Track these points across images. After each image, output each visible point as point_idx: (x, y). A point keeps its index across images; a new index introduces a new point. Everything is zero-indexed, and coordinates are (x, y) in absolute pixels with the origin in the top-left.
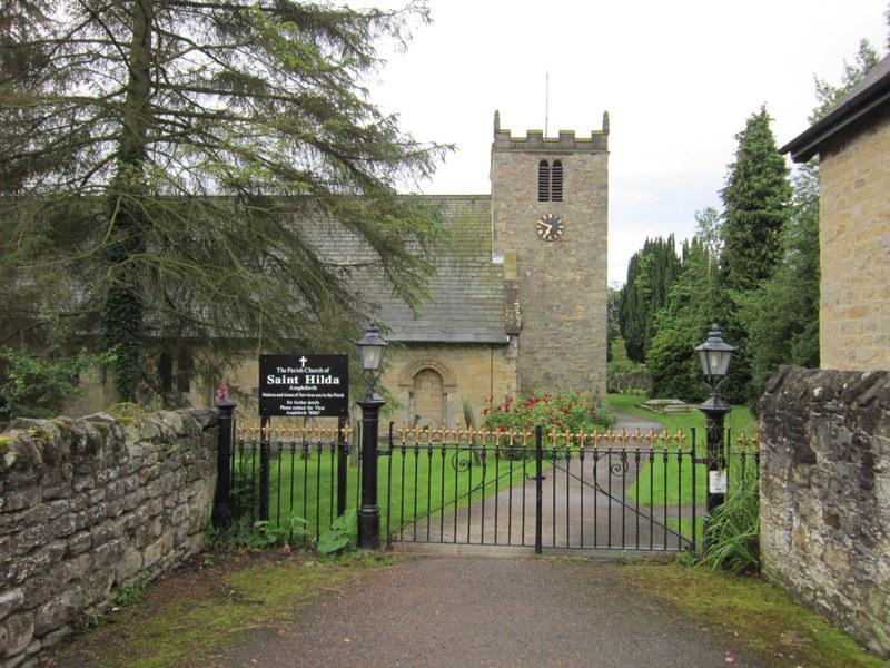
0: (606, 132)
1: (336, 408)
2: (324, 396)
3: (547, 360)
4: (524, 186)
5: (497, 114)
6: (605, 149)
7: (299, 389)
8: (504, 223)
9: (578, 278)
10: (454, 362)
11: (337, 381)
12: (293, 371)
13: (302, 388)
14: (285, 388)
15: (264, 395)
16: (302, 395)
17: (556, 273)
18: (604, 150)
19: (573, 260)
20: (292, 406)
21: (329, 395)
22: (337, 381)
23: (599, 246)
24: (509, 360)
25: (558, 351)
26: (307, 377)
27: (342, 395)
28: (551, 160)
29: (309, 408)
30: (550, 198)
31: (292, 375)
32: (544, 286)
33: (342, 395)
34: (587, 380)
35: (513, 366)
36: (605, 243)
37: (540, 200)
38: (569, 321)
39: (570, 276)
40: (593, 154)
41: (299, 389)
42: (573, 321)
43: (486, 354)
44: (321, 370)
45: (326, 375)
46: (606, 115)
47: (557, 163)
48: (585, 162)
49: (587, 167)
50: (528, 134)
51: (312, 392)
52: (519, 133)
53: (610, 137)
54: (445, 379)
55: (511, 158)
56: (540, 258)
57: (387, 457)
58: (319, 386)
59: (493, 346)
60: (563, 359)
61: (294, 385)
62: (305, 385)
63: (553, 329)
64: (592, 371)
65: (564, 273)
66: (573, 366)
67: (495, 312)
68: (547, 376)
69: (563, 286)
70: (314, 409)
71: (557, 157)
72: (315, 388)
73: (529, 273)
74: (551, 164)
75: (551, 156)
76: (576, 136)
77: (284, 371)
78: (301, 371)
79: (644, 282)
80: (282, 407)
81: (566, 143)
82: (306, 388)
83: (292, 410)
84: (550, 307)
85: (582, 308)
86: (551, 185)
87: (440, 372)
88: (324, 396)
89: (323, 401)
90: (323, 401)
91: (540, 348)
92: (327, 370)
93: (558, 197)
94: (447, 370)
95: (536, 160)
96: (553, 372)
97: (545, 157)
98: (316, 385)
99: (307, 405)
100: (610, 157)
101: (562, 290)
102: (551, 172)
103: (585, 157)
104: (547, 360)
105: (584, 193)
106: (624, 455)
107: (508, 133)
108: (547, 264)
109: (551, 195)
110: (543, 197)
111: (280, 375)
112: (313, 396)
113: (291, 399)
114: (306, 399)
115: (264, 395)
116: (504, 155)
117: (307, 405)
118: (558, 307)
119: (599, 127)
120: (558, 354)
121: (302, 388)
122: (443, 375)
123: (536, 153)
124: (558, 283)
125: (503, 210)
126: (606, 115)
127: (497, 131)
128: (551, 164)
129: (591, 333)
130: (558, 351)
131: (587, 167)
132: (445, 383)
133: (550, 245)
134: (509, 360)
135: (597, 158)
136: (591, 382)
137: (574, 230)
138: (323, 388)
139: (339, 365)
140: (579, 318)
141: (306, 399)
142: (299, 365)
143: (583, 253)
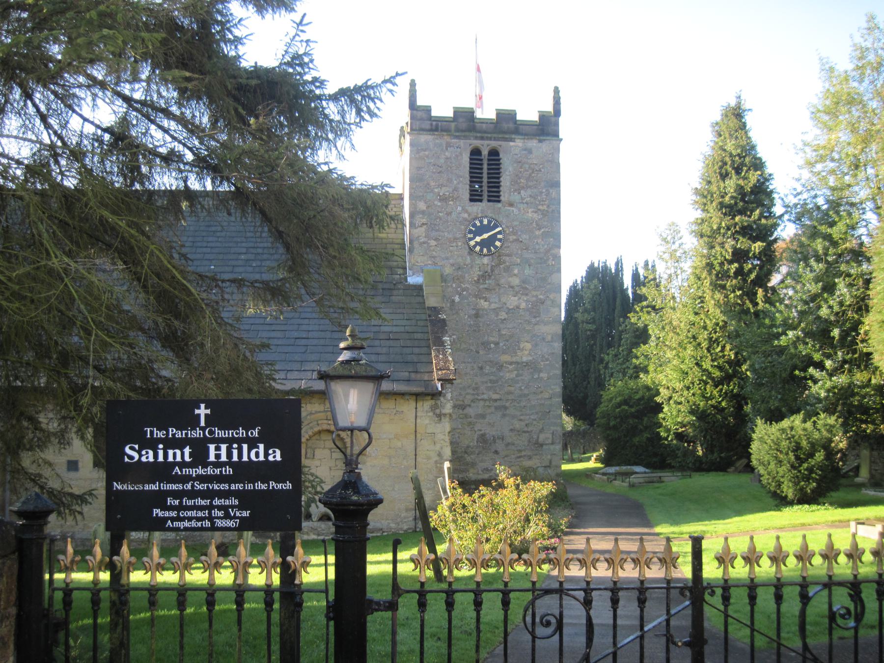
0: (557, 112)
2: (250, 487)
3: (483, 416)
4: (450, 180)
6: (556, 134)
8: (423, 229)
9: (523, 305)
12: (179, 435)
13: (200, 471)
14: (162, 471)
16: (199, 487)
18: (554, 134)
20: (178, 508)
22: (276, 455)
23: (550, 262)
24: (440, 416)
25: (498, 404)
26: (212, 447)
27: (289, 486)
29: (217, 513)
30: (485, 197)
31: (179, 444)
32: (477, 316)
33: (289, 486)
34: (537, 443)
35: (446, 426)
36: (557, 258)
37: (471, 200)
38: (511, 363)
39: (512, 301)
40: (540, 141)
42: (518, 363)
44: (242, 433)
46: (556, 91)
47: (494, 153)
48: (530, 151)
50: (455, 112)
51: (220, 479)
52: (443, 110)
53: (561, 120)
57: (389, 614)
60: (504, 415)
61: (183, 464)
62: (205, 465)
64: (542, 431)
66: (517, 425)
67: (416, 350)
68: (483, 438)
70: (227, 516)
71: (494, 144)
72: (229, 471)
73: (457, 299)
74: (485, 152)
75: (486, 142)
76: (519, 118)
77: (161, 434)
78: (197, 434)
79: (586, 315)
80: (157, 512)
81: (505, 126)
82: (210, 471)
83: (179, 519)
84: (485, 344)
85: (528, 346)
88: (250, 487)
92: (256, 433)
93: (495, 197)
96: (490, 432)
97: (477, 143)
98: (230, 463)
99: (211, 507)
100: (562, 146)
102: (485, 163)
104: (483, 416)
105: (529, 192)
107: (428, 110)
109: (485, 194)
110: (475, 197)
111: (153, 444)
112: (224, 487)
114: (208, 494)
117: (211, 507)
118: (497, 344)
119: (549, 108)
120: (496, 408)
121: (200, 471)
123: (466, 137)
124: (496, 311)
125: (423, 212)
126: (556, 91)
127: (413, 105)
128: (485, 152)
130: (498, 404)
133: (486, 260)
135: (545, 147)
136: (542, 445)
137: (517, 240)
138: (245, 471)
140: (525, 359)
141: (208, 494)
142: (194, 422)
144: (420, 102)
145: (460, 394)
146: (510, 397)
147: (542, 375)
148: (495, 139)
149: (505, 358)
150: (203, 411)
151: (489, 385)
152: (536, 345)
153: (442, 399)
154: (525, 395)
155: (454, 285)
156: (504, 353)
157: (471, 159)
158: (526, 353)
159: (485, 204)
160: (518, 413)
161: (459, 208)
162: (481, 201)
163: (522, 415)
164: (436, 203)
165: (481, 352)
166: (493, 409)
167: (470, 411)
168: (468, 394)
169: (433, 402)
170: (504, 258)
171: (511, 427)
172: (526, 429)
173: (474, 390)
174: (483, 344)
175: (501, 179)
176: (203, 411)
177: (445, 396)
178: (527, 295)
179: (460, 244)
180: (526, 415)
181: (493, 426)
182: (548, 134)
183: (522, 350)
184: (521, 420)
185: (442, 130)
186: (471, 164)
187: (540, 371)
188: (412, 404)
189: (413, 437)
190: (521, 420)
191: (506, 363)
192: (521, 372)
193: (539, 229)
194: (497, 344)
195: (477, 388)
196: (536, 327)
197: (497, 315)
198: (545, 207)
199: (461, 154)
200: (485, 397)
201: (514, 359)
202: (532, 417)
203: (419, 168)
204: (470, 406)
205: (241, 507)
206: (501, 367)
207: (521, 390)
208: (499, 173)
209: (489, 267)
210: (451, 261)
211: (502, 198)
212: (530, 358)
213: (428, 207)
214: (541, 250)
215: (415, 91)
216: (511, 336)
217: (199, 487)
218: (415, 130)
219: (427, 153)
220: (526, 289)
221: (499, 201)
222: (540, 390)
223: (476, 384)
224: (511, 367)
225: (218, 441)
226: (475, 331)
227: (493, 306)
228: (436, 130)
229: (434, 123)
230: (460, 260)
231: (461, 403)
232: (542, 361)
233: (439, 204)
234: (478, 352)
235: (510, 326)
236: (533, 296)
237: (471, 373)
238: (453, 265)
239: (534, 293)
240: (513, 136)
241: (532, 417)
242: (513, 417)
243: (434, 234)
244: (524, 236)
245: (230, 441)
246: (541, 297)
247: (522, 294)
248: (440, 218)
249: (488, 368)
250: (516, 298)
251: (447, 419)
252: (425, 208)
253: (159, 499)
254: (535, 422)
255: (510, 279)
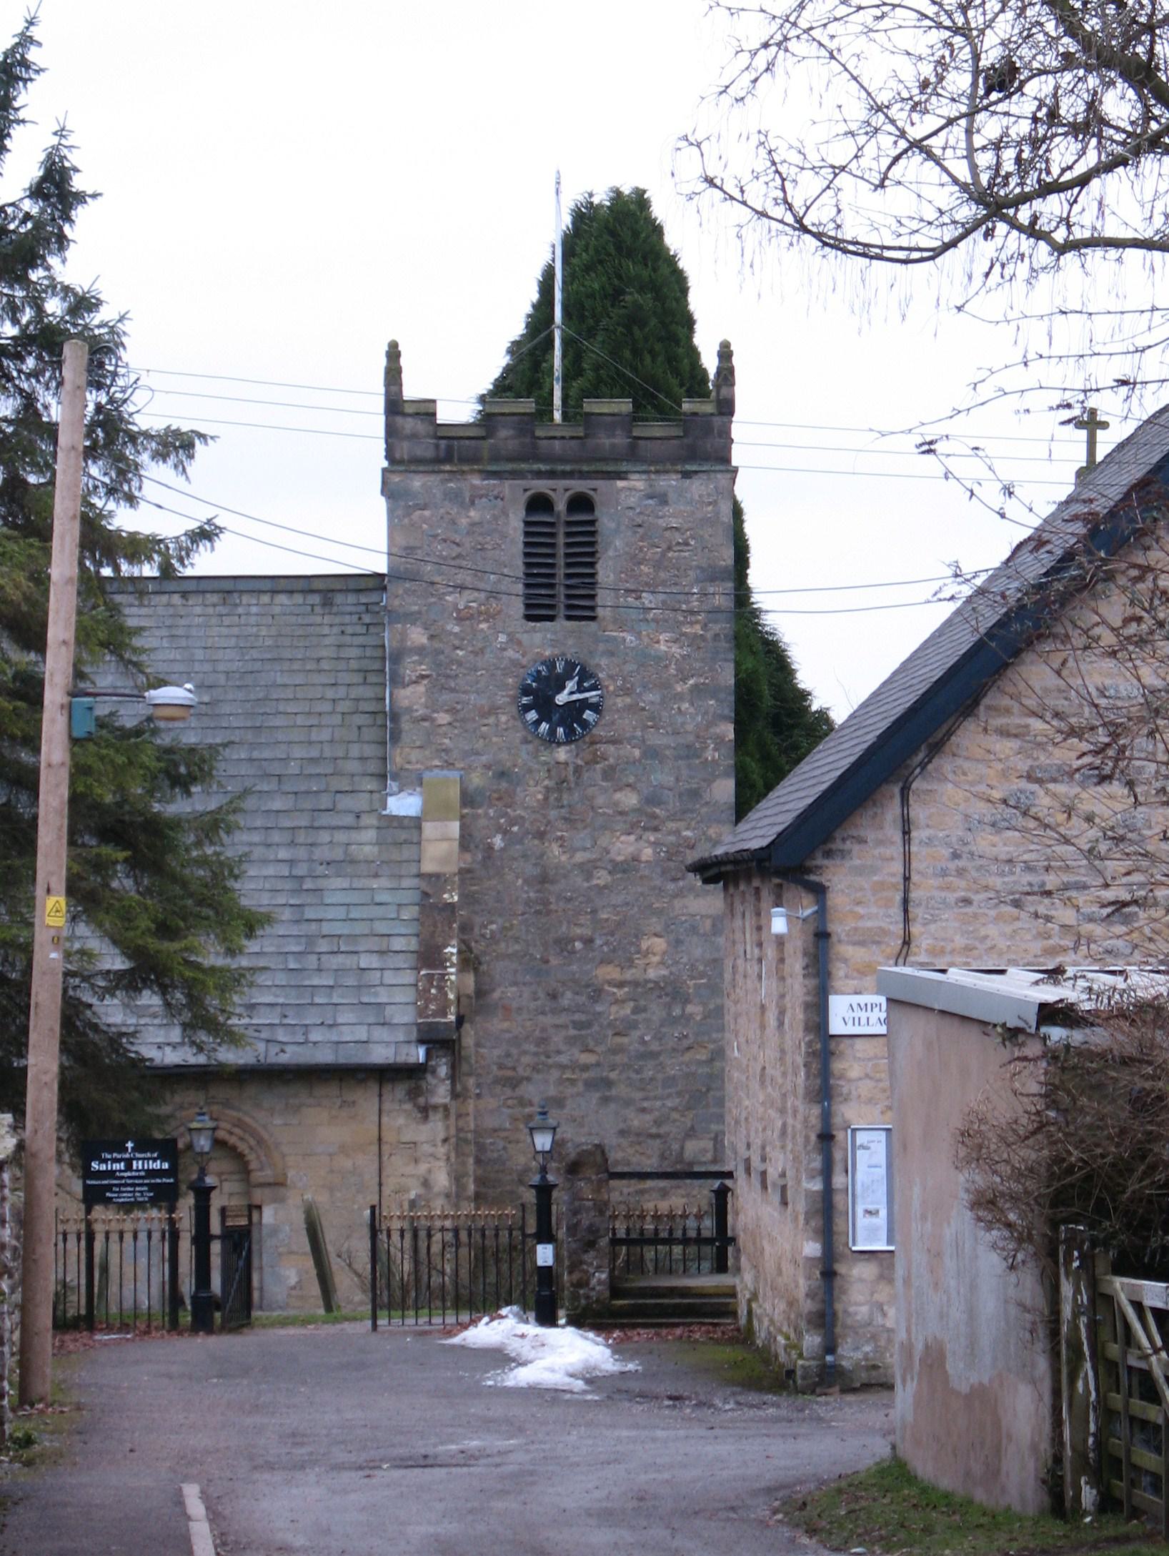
1: (165, 1196)
5: (393, 353)
6: (723, 457)
7: (126, 1174)
8: (421, 688)
9: (647, 853)
10: (278, 1121)
11: (166, 1166)
12: (119, 1156)
13: (128, 1174)
14: (111, 1174)
15: (89, 1182)
16: (129, 1181)
17: (581, 837)
19: (630, 799)
21: (158, 1181)
28: (560, 492)
32: (544, 879)
37: (529, 618)
38: (621, 985)
39: (623, 846)
40: (687, 475)
41: (126, 1174)
42: (636, 984)
43: (366, 1099)
44: (149, 1155)
45: (155, 1160)
47: (582, 503)
48: (663, 499)
49: (672, 516)
54: (253, 1166)
55: (438, 492)
56: (532, 794)
58: (148, 1170)
59: (385, 1075)
60: (605, 1100)
61: (120, 1171)
63: (579, 1009)
64: (691, 1133)
65: (604, 841)
66: (636, 1122)
69: (602, 878)
71: (579, 486)
72: (142, 1174)
73: (498, 841)
75: (561, 484)
77: (109, 1156)
78: (127, 1156)
80: (108, 1194)
82: (134, 1174)
84: (563, 944)
85: (659, 944)
86: (561, 571)
87: (242, 1147)
89: (152, 1187)
90: (152, 1187)
91: (535, 1069)
93: (582, 608)
94: (260, 1141)
95: (515, 493)
97: (542, 486)
98: (143, 1170)
101: (601, 889)
103: (669, 482)
106: (483, 1231)
108: (553, 814)
110: (537, 612)
111: (105, 1161)
112: (140, 1181)
113: (116, 1185)
114: (134, 1185)
115: (89, 1182)
116: (417, 482)
117: (134, 1192)
120: (590, 1084)
121: (128, 1174)
122: (251, 1157)
123: (515, 475)
124: (587, 870)
125: (420, 650)
127: (395, 405)
129: (687, 1018)
131: (672, 516)
132: (257, 1176)
133: (562, 754)
134: (425, 1112)
137: (632, 709)
138: (151, 1173)
139: (168, 1149)
140: (652, 974)
141: (134, 1185)
143: (662, 777)
144: (412, 390)
145: (508, 1055)
146: (618, 1059)
147: (690, 1009)
148: (582, 475)
149: (610, 972)
150: (130, 1145)
151: (572, 1032)
152: (678, 942)
153: (429, 1077)
154: (654, 1055)
155: (491, 812)
156: (605, 961)
157: (527, 523)
158: (656, 959)
159: (561, 625)
160: (639, 1095)
161: (502, 638)
162: (551, 618)
163: (646, 1099)
164: (449, 627)
165: (554, 961)
166: (580, 1087)
167: (528, 1090)
168: (525, 1052)
169: (412, 1084)
170: (603, 747)
171: (622, 1126)
172: (654, 1130)
173: (538, 1045)
174: (558, 941)
175: (598, 566)
176: (130, 1145)
177: (434, 1072)
178: (656, 829)
179: (503, 718)
180: (656, 1098)
181: (582, 1125)
182: (706, 458)
183: (647, 953)
184: (643, 1110)
185: (463, 460)
186: (527, 534)
187: (687, 1001)
188: (374, 1088)
189: (375, 1148)
190: (643, 1110)
191: (610, 983)
192: (642, 1003)
193: (684, 680)
194: (588, 941)
195: (543, 1041)
196: (678, 903)
197: (589, 877)
198: (697, 629)
199: (505, 513)
200: (563, 1059)
201: (629, 975)
202: (669, 1103)
203: (410, 550)
204: (528, 1079)
205: (149, 1191)
206: (597, 994)
207: (644, 1043)
208: (593, 554)
209: (571, 768)
210: (484, 759)
211: (600, 612)
212: (665, 972)
213: (432, 637)
214: (690, 727)
215: (399, 371)
216: (620, 924)
217: (129, 1181)
218: (401, 462)
219: (427, 513)
220: (654, 816)
221: (593, 618)
222: (686, 1043)
223: (544, 1030)
224: (621, 993)
225: (138, 1159)
226: (538, 912)
227: (580, 857)
228: (448, 459)
229: (443, 443)
230: (504, 756)
231: (510, 1073)
232: (692, 978)
233: (457, 629)
234: (547, 962)
235: (619, 899)
236: (670, 833)
237: (533, 1005)
238: (487, 767)
239: (672, 825)
240: (624, 467)
241: (669, 1103)
242: (628, 1103)
243: (446, 697)
244: (651, 697)
245: (143, 1159)
246: (688, 833)
247: (645, 829)
248: (460, 664)
249: (569, 994)
250: (632, 838)
251: (440, 1115)
252: (424, 640)
253: (109, 1188)
254: (675, 1115)
255: (618, 796)
